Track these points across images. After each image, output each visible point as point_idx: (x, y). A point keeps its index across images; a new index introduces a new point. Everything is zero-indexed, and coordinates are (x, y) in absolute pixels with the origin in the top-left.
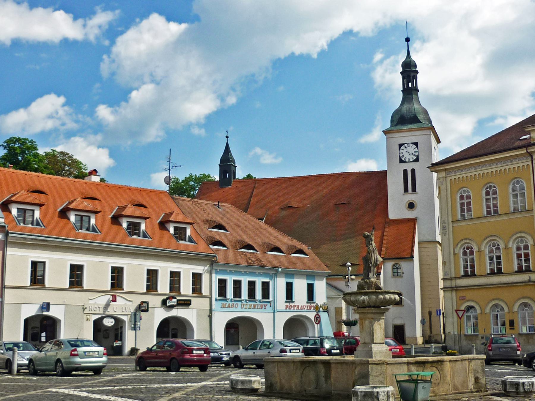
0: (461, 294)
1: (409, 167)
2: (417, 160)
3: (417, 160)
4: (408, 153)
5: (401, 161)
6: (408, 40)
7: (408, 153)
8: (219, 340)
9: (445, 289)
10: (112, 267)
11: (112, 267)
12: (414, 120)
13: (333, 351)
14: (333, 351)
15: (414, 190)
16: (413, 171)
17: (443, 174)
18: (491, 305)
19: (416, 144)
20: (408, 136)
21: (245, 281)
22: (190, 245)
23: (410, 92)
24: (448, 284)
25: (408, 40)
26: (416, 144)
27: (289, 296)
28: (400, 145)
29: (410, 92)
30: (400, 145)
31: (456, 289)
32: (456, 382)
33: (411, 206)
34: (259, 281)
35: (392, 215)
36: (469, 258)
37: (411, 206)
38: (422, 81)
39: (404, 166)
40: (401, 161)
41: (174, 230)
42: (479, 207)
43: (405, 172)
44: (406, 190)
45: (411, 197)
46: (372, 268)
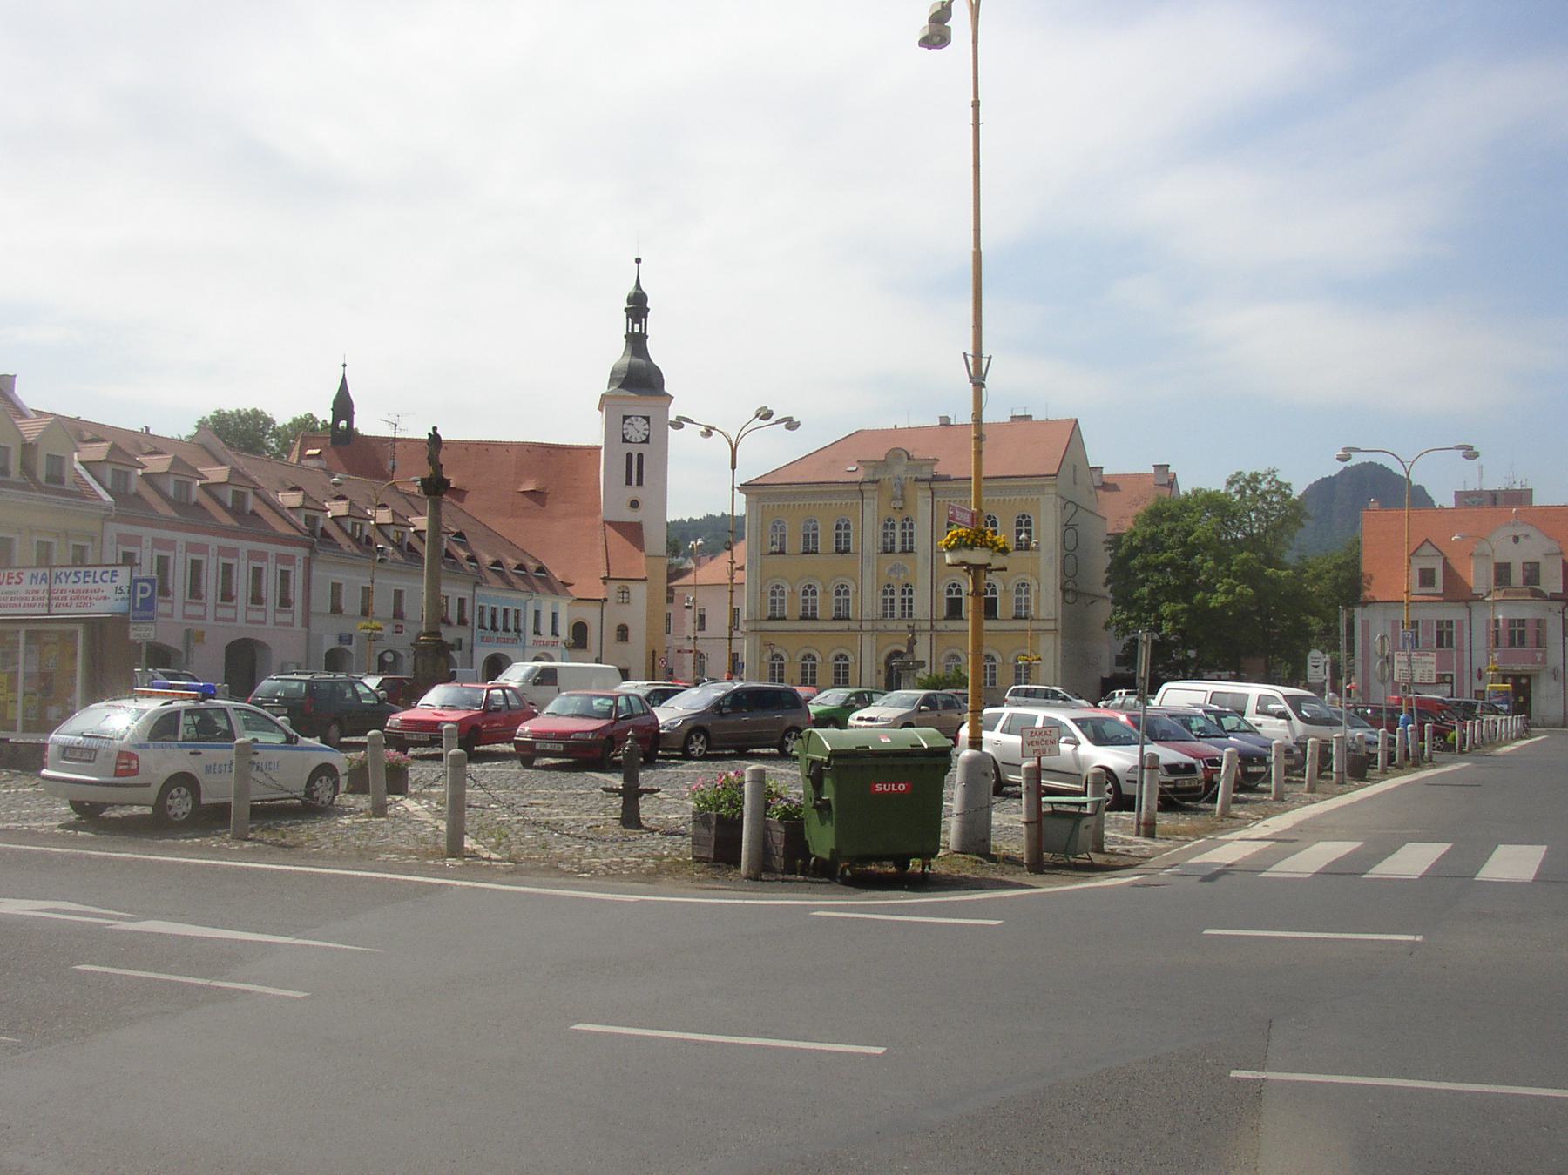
1: (635, 450)
2: (647, 441)
3: (647, 441)
4: (637, 430)
5: (625, 440)
6: (638, 261)
7: (637, 430)
8: (1416, 588)
9: (963, 682)
13: (561, 865)
14: (561, 865)
15: (640, 482)
16: (640, 456)
18: (948, 652)
19: (647, 419)
20: (638, 405)
25: (638, 261)
29: (637, 342)
30: (625, 418)
32: (346, 821)
33: (634, 504)
37: (634, 504)
39: (628, 448)
41: (216, 806)
43: (629, 456)
44: (629, 482)
45: (634, 492)
46: (1118, 710)
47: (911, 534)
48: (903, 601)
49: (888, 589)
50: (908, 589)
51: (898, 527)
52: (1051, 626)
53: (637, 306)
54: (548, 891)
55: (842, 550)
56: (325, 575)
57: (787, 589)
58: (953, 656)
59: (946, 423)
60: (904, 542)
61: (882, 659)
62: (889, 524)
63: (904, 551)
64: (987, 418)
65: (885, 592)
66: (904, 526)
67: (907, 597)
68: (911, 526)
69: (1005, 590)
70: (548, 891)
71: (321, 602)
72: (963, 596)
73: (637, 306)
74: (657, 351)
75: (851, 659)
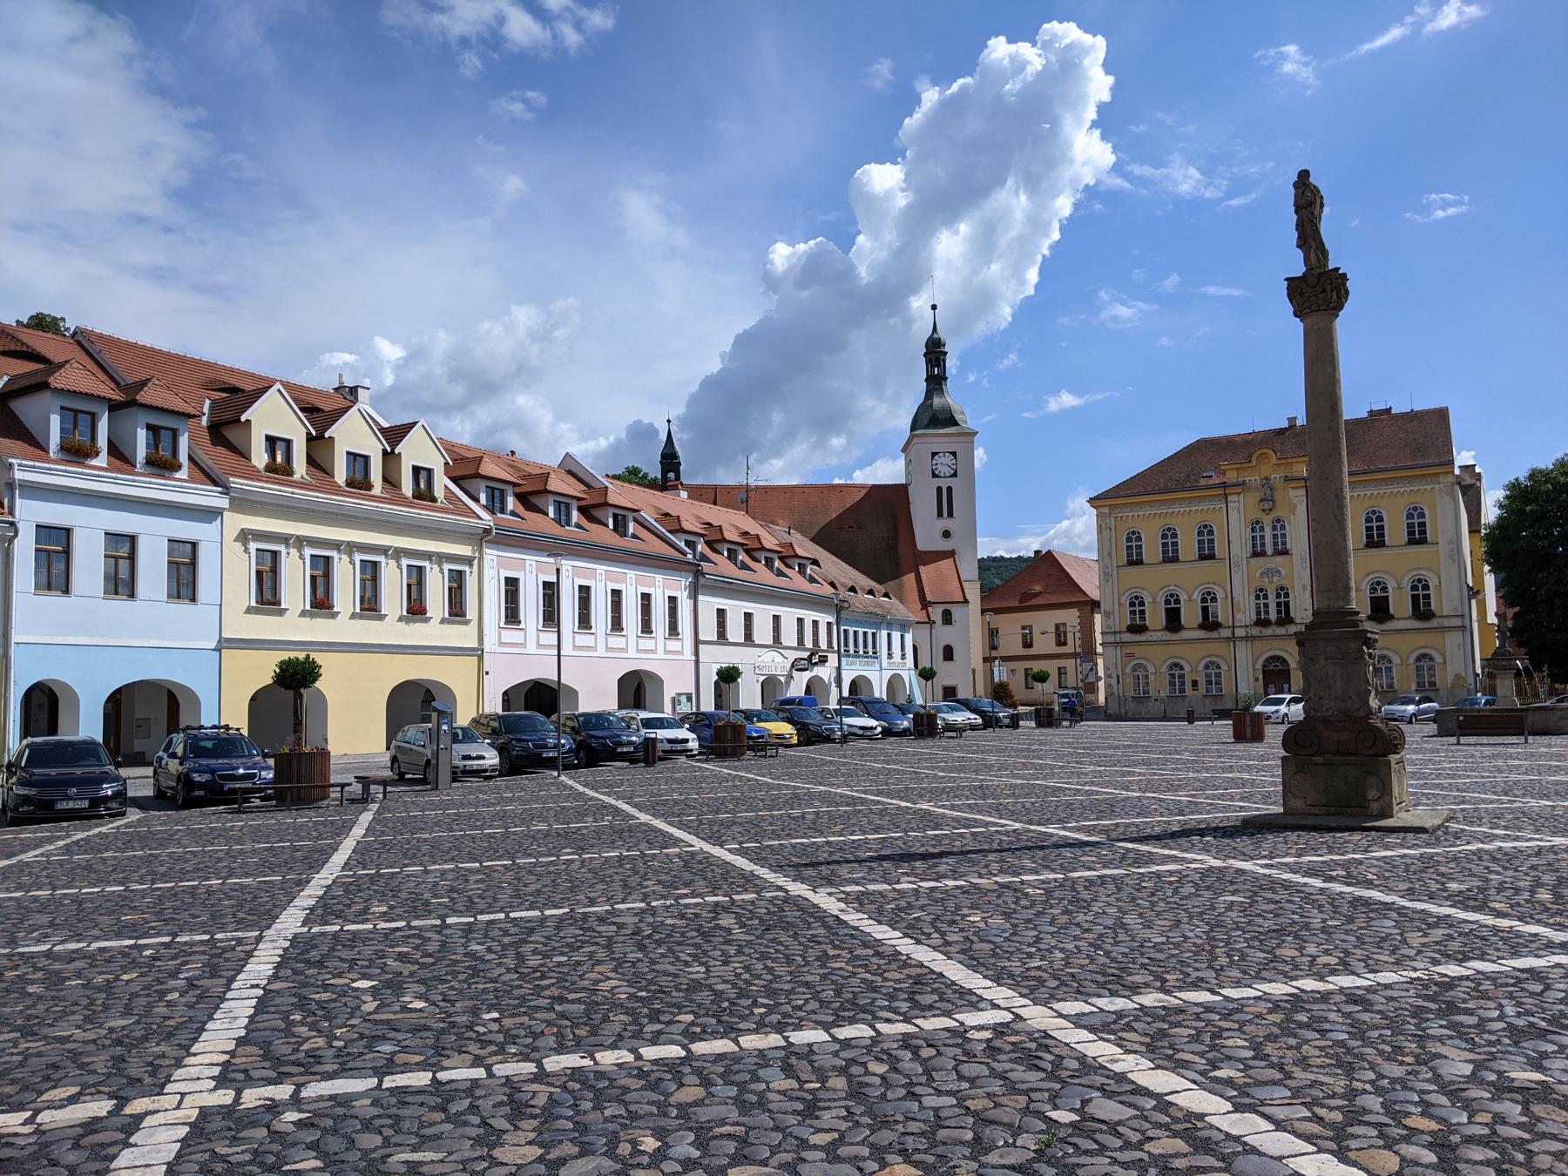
0: (1127, 650)
2: (955, 475)
3: (955, 475)
4: (944, 464)
5: (934, 475)
6: (934, 307)
7: (944, 464)
10: (1441, 415)
11: (1441, 415)
12: (952, 421)
15: (950, 514)
16: (950, 489)
17: (1106, 510)
18: (1203, 664)
19: (954, 454)
20: (939, 439)
21: (861, 631)
22: (1371, 40)
23: (936, 381)
24: (1111, 638)
25: (934, 307)
26: (954, 454)
27: (890, 656)
28: (934, 454)
29: (936, 381)
30: (934, 454)
31: (1122, 644)
33: (946, 534)
34: (870, 631)
35: (923, 544)
36: (1262, 601)
37: (946, 534)
38: (951, 363)
40: (934, 475)
42: (1152, 550)
43: (939, 489)
44: (940, 514)
45: (945, 523)
47: (1284, 536)
48: (1279, 604)
49: (1261, 593)
50: (1282, 591)
51: (1268, 539)
52: (1457, 622)
53: (1307, 199)
54: (53, 772)
55: (1207, 556)
56: (709, 604)
57: (1183, 597)
58: (1176, 665)
59: (1292, 426)
60: (1275, 544)
61: (1259, 665)
62: (1256, 526)
63: (1277, 553)
64: (1353, 407)
65: (1258, 597)
66: (1274, 528)
67: (1262, 601)
68: (1283, 527)
69: (1400, 588)
70: (53, 772)
71: (709, 631)
72: (1390, 594)
73: (1307, 199)
74: (952, 397)
75: (1224, 667)
